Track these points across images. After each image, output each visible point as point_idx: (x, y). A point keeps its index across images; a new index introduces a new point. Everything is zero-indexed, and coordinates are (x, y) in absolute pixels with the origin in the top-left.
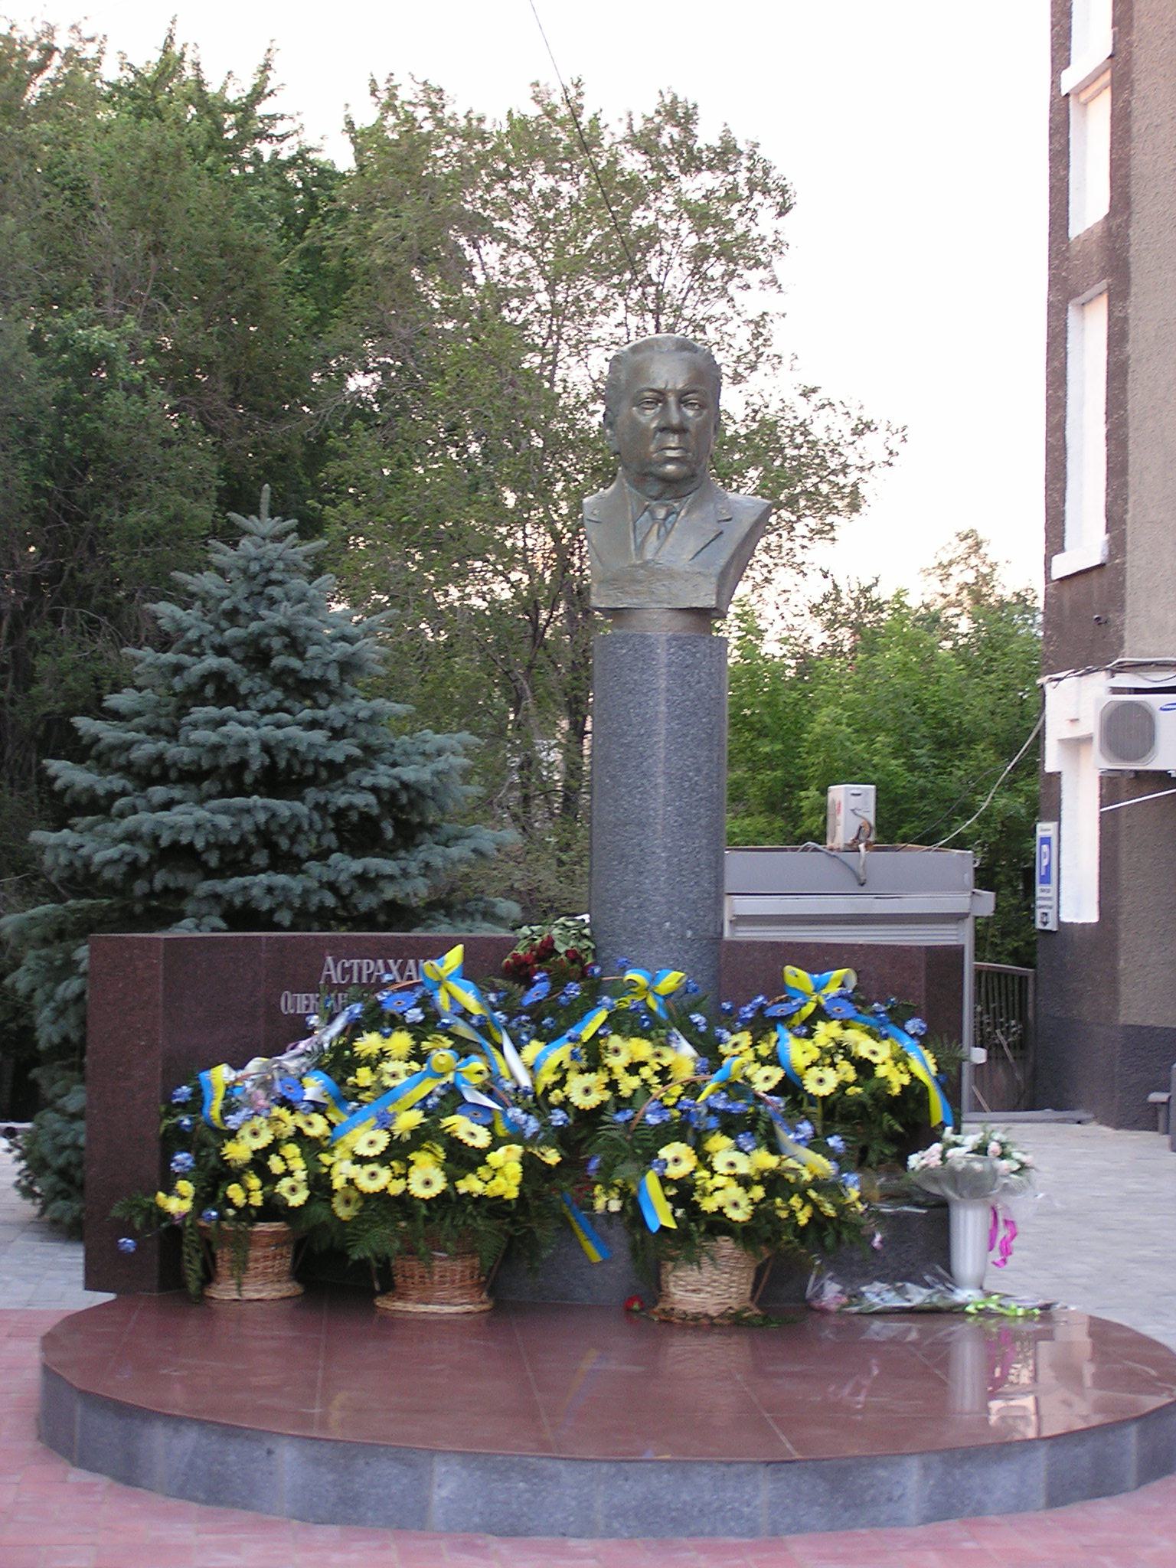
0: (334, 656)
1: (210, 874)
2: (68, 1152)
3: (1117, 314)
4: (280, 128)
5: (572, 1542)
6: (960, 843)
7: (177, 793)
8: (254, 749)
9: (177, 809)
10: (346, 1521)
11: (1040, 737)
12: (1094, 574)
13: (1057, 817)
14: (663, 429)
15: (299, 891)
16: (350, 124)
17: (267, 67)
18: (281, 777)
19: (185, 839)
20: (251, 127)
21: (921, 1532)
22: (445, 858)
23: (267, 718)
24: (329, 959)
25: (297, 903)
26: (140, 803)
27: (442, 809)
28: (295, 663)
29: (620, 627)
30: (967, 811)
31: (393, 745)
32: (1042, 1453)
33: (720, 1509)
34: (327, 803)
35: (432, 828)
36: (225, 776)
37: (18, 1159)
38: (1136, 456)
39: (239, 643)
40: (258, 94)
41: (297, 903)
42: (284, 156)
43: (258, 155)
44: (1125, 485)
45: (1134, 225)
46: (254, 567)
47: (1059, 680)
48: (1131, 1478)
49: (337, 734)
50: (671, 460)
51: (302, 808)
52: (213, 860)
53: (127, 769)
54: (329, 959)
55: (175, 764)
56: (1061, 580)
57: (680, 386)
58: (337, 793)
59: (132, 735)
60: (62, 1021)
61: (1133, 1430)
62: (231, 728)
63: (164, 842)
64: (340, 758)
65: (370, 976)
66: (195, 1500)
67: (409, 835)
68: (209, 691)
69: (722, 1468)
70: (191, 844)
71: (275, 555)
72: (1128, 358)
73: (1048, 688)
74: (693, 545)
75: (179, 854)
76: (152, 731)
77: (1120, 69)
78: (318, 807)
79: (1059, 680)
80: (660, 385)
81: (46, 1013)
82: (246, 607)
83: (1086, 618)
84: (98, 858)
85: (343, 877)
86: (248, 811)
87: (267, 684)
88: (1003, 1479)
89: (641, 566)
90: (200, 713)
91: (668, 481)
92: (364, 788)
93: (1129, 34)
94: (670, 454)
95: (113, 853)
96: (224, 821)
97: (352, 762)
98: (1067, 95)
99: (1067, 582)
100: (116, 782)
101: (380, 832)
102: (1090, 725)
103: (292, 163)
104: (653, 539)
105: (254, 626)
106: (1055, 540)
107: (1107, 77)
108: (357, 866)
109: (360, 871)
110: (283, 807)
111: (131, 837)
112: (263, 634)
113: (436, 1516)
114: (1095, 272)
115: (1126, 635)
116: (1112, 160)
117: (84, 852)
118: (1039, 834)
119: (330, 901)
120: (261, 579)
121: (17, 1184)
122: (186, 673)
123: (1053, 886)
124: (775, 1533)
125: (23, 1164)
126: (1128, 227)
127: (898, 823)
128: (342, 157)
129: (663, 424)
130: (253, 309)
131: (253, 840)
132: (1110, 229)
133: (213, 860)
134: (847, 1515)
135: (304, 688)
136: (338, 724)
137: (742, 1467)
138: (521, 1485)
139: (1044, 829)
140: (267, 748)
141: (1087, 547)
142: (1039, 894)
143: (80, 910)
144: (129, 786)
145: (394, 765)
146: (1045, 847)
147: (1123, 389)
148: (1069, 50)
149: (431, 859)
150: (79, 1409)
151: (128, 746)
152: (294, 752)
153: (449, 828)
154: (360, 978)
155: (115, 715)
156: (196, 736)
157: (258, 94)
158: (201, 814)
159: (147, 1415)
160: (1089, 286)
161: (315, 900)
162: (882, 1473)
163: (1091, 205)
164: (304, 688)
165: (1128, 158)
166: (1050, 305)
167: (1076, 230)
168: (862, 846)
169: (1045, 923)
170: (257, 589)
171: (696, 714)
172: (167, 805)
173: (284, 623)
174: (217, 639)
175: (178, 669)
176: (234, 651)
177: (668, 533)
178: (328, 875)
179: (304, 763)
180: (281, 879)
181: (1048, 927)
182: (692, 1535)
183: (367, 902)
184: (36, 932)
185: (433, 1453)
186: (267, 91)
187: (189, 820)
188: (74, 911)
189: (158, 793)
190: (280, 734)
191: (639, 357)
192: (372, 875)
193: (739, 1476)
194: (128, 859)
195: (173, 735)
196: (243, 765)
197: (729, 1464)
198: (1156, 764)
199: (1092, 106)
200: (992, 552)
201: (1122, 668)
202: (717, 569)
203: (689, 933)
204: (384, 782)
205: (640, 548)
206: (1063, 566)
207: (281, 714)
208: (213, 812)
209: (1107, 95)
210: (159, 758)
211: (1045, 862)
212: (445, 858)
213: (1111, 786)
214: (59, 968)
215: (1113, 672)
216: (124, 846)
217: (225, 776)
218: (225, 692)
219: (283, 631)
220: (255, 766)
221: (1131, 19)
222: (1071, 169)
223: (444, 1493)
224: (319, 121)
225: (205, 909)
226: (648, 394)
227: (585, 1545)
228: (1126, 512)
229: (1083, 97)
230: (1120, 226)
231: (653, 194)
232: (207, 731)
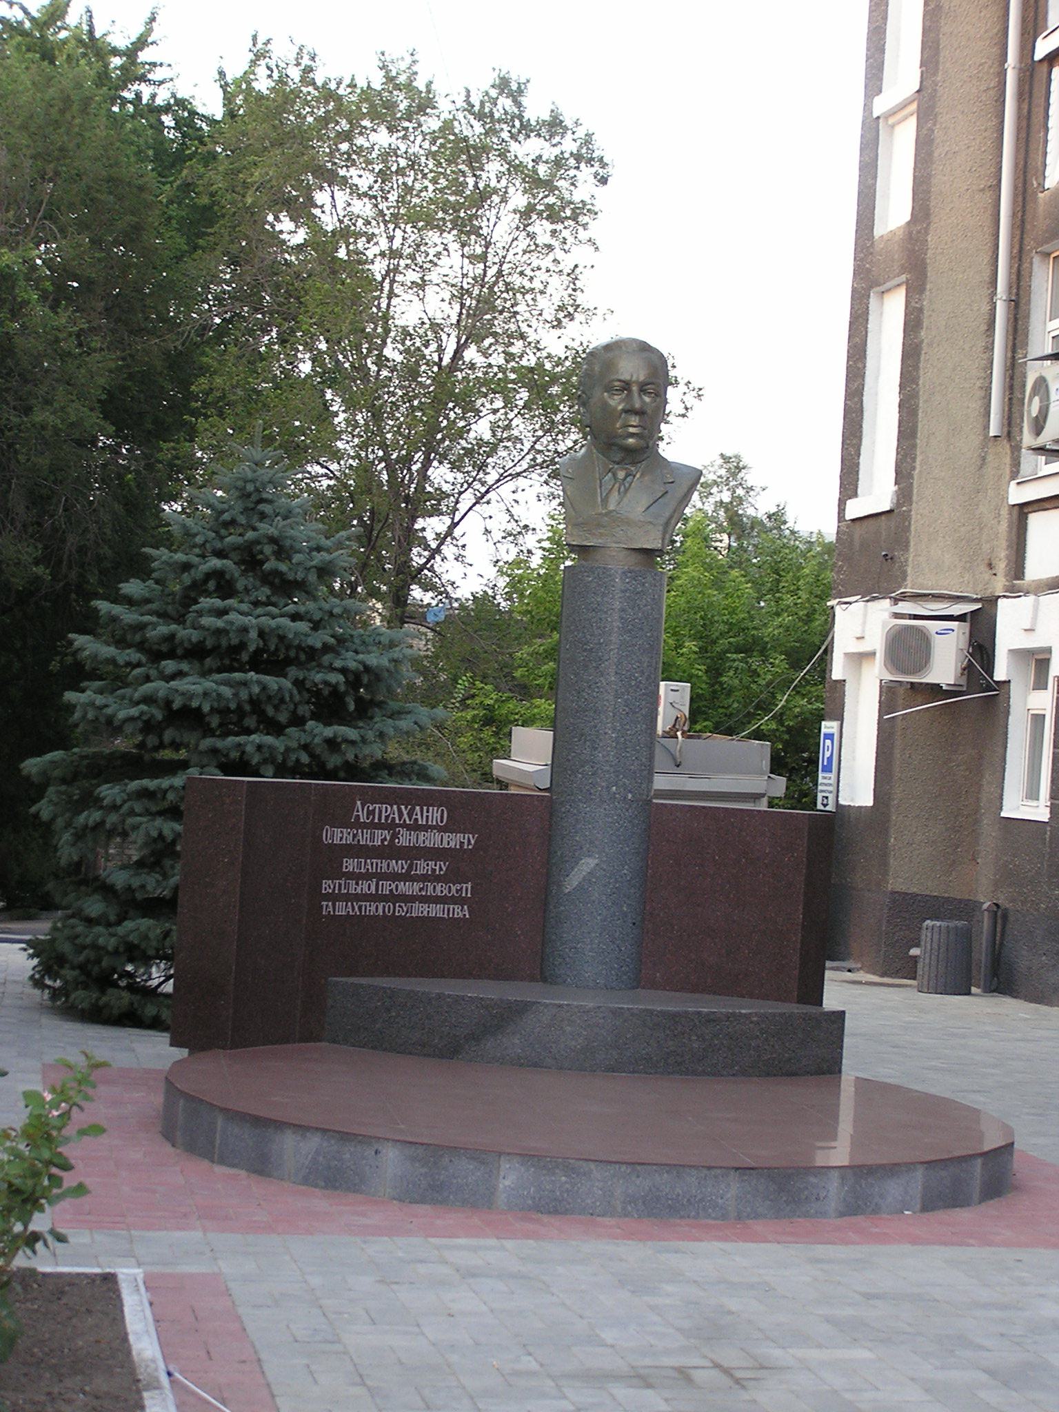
0: (314, 563)
1: (208, 732)
2: (87, 951)
3: (913, 304)
4: (157, 75)
5: (599, 1219)
6: (758, 735)
7: (185, 666)
8: (253, 634)
9: (186, 680)
10: (434, 1202)
11: (828, 651)
12: (883, 517)
13: (840, 718)
14: (626, 411)
15: (282, 749)
16: (222, 74)
17: (153, 19)
18: (273, 657)
19: (195, 704)
20: (133, 72)
21: (838, 1221)
22: (396, 728)
23: (260, 610)
24: (359, 803)
25: (280, 759)
26: (153, 673)
27: (390, 690)
28: (283, 567)
29: (585, 560)
30: (764, 707)
31: (352, 636)
32: (919, 1173)
33: (701, 1200)
34: (305, 679)
35: (380, 705)
36: (219, 654)
37: (32, 956)
38: (924, 425)
39: (236, 548)
40: (142, 43)
41: (280, 759)
42: (159, 101)
43: (138, 96)
44: (914, 446)
45: (931, 233)
46: (250, 487)
47: (850, 603)
48: (976, 1195)
49: (316, 625)
50: (632, 435)
51: (287, 684)
52: (215, 721)
53: (141, 646)
54: (359, 803)
55: (182, 642)
56: (853, 520)
57: (642, 378)
58: (313, 673)
59: (147, 618)
60: (80, 844)
61: (979, 1161)
62: (233, 616)
63: (176, 706)
64: (319, 645)
65: (387, 817)
66: (316, 1186)
67: (364, 710)
68: (211, 585)
69: (705, 1171)
70: (199, 709)
71: (266, 479)
72: (922, 341)
73: (838, 610)
74: (645, 502)
75: (187, 716)
76: (162, 615)
77: (926, 102)
78: (299, 683)
79: (850, 603)
80: (626, 377)
81: (67, 836)
82: (242, 519)
83: (871, 555)
84: (122, 715)
85: (317, 740)
86: (245, 684)
87: (258, 583)
88: (894, 1189)
89: (606, 515)
90: (206, 602)
91: (628, 450)
92: (335, 669)
93: (935, 74)
94: (631, 430)
95: (134, 712)
96: (227, 691)
97: (326, 648)
98: (878, 118)
99: (858, 523)
100: (134, 655)
101: (344, 705)
102: (876, 642)
103: (167, 109)
104: (615, 495)
105: (250, 535)
106: (849, 485)
107: (914, 106)
108: (329, 732)
109: (331, 735)
110: (272, 682)
111: (148, 700)
112: (257, 542)
113: (501, 1199)
114: (896, 267)
115: (909, 570)
116: (915, 177)
117: (109, 711)
118: (823, 730)
119: (305, 759)
120: (254, 498)
121: (32, 977)
122: (193, 571)
123: (833, 775)
124: (739, 1218)
125: (36, 961)
126: (927, 234)
127: (709, 714)
128: (211, 104)
129: (628, 407)
130: (132, 237)
131: (247, 708)
132: (910, 233)
133: (215, 721)
134: (789, 1208)
135: (285, 586)
136: (317, 616)
137: (719, 1171)
138: (563, 1178)
139: (828, 727)
140: (261, 634)
141: (877, 494)
142: (820, 780)
143: (86, 757)
144: (144, 659)
145: (356, 652)
146: (828, 742)
147: (916, 367)
148: (881, 79)
149: (385, 730)
150: (220, 1122)
151: (142, 627)
152: (282, 638)
153: (393, 705)
154: (380, 819)
155: (130, 601)
156: (206, 621)
157: (142, 43)
158: (208, 684)
159: (280, 1125)
160: (889, 279)
161: (293, 757)
162: (813, 1180)
163: (895, 212)
164: (285, 586)
165: (929, 176)
166: (854, 290)
167: (879, 231)
168: (679, 733)
169: (825, 805)
170: (252, 505)
171: (641, 629)
172: (179, 674)
173: (276, 533)
174: (219, 545)
175: (186, 567)
176: (233, 555)
177: (626, 490)
178: (305, 738)
179: (288, 648)
180: (269, 740)
181: (827, 808)
182: (682, 1217)
183: (333, 761)
184: (57, 773)
185: (500, 1154)
186: (150, 40)
187: (198, 689)
188: (83, 757)
189: (169, 666)
190: (273, 623)
191: (610, 355)
192: (339, 740)
193: (716, 1177)
194: (145, 718)
195: (180, 620)
196: (242, 646)
197: (709, 1168)
198: (930, 679)
199: (898, 129)
200: (750, 478)
201: (904, 597)
202: (662, 520)
203: (630, 796)
204: (352, 665)
205: (605, 501)
206: (855, 509)
207: (270, 608)
208: (216, 682)
209: (913, 121)
210: (172, 636)
211: (827, 754)
212: (396, 728)
213: (889, 696)
214: (77, 801)
215: (896, 601)
216: (143, 707)
217: (219, 654)
218: (225, 588)
219: (273, 540)
220: (252, 648)
221: (937, 62)
222: (878, 179)
223: (507, 1183)
224: (193, 73)
225: (205, 761)
226: (617, 383)
227: (607, 1221)
228: (914, 468)
229: (891, 121)
230: (919, 232)
231: (497, 165)
232: (210, 617)
